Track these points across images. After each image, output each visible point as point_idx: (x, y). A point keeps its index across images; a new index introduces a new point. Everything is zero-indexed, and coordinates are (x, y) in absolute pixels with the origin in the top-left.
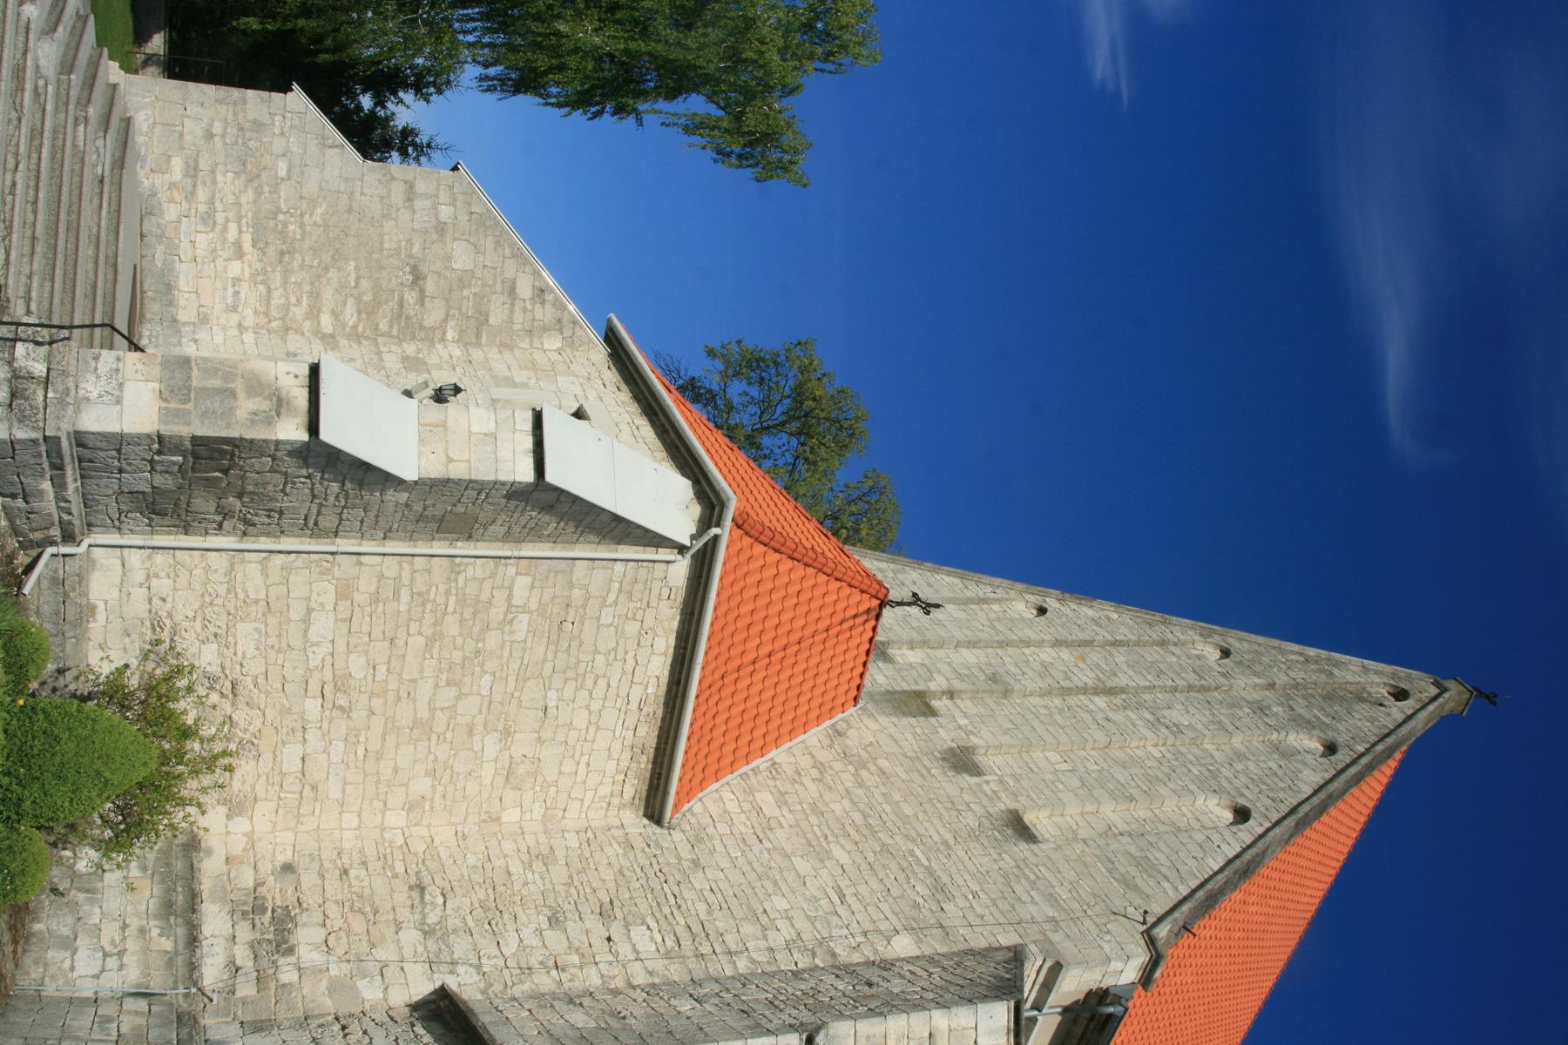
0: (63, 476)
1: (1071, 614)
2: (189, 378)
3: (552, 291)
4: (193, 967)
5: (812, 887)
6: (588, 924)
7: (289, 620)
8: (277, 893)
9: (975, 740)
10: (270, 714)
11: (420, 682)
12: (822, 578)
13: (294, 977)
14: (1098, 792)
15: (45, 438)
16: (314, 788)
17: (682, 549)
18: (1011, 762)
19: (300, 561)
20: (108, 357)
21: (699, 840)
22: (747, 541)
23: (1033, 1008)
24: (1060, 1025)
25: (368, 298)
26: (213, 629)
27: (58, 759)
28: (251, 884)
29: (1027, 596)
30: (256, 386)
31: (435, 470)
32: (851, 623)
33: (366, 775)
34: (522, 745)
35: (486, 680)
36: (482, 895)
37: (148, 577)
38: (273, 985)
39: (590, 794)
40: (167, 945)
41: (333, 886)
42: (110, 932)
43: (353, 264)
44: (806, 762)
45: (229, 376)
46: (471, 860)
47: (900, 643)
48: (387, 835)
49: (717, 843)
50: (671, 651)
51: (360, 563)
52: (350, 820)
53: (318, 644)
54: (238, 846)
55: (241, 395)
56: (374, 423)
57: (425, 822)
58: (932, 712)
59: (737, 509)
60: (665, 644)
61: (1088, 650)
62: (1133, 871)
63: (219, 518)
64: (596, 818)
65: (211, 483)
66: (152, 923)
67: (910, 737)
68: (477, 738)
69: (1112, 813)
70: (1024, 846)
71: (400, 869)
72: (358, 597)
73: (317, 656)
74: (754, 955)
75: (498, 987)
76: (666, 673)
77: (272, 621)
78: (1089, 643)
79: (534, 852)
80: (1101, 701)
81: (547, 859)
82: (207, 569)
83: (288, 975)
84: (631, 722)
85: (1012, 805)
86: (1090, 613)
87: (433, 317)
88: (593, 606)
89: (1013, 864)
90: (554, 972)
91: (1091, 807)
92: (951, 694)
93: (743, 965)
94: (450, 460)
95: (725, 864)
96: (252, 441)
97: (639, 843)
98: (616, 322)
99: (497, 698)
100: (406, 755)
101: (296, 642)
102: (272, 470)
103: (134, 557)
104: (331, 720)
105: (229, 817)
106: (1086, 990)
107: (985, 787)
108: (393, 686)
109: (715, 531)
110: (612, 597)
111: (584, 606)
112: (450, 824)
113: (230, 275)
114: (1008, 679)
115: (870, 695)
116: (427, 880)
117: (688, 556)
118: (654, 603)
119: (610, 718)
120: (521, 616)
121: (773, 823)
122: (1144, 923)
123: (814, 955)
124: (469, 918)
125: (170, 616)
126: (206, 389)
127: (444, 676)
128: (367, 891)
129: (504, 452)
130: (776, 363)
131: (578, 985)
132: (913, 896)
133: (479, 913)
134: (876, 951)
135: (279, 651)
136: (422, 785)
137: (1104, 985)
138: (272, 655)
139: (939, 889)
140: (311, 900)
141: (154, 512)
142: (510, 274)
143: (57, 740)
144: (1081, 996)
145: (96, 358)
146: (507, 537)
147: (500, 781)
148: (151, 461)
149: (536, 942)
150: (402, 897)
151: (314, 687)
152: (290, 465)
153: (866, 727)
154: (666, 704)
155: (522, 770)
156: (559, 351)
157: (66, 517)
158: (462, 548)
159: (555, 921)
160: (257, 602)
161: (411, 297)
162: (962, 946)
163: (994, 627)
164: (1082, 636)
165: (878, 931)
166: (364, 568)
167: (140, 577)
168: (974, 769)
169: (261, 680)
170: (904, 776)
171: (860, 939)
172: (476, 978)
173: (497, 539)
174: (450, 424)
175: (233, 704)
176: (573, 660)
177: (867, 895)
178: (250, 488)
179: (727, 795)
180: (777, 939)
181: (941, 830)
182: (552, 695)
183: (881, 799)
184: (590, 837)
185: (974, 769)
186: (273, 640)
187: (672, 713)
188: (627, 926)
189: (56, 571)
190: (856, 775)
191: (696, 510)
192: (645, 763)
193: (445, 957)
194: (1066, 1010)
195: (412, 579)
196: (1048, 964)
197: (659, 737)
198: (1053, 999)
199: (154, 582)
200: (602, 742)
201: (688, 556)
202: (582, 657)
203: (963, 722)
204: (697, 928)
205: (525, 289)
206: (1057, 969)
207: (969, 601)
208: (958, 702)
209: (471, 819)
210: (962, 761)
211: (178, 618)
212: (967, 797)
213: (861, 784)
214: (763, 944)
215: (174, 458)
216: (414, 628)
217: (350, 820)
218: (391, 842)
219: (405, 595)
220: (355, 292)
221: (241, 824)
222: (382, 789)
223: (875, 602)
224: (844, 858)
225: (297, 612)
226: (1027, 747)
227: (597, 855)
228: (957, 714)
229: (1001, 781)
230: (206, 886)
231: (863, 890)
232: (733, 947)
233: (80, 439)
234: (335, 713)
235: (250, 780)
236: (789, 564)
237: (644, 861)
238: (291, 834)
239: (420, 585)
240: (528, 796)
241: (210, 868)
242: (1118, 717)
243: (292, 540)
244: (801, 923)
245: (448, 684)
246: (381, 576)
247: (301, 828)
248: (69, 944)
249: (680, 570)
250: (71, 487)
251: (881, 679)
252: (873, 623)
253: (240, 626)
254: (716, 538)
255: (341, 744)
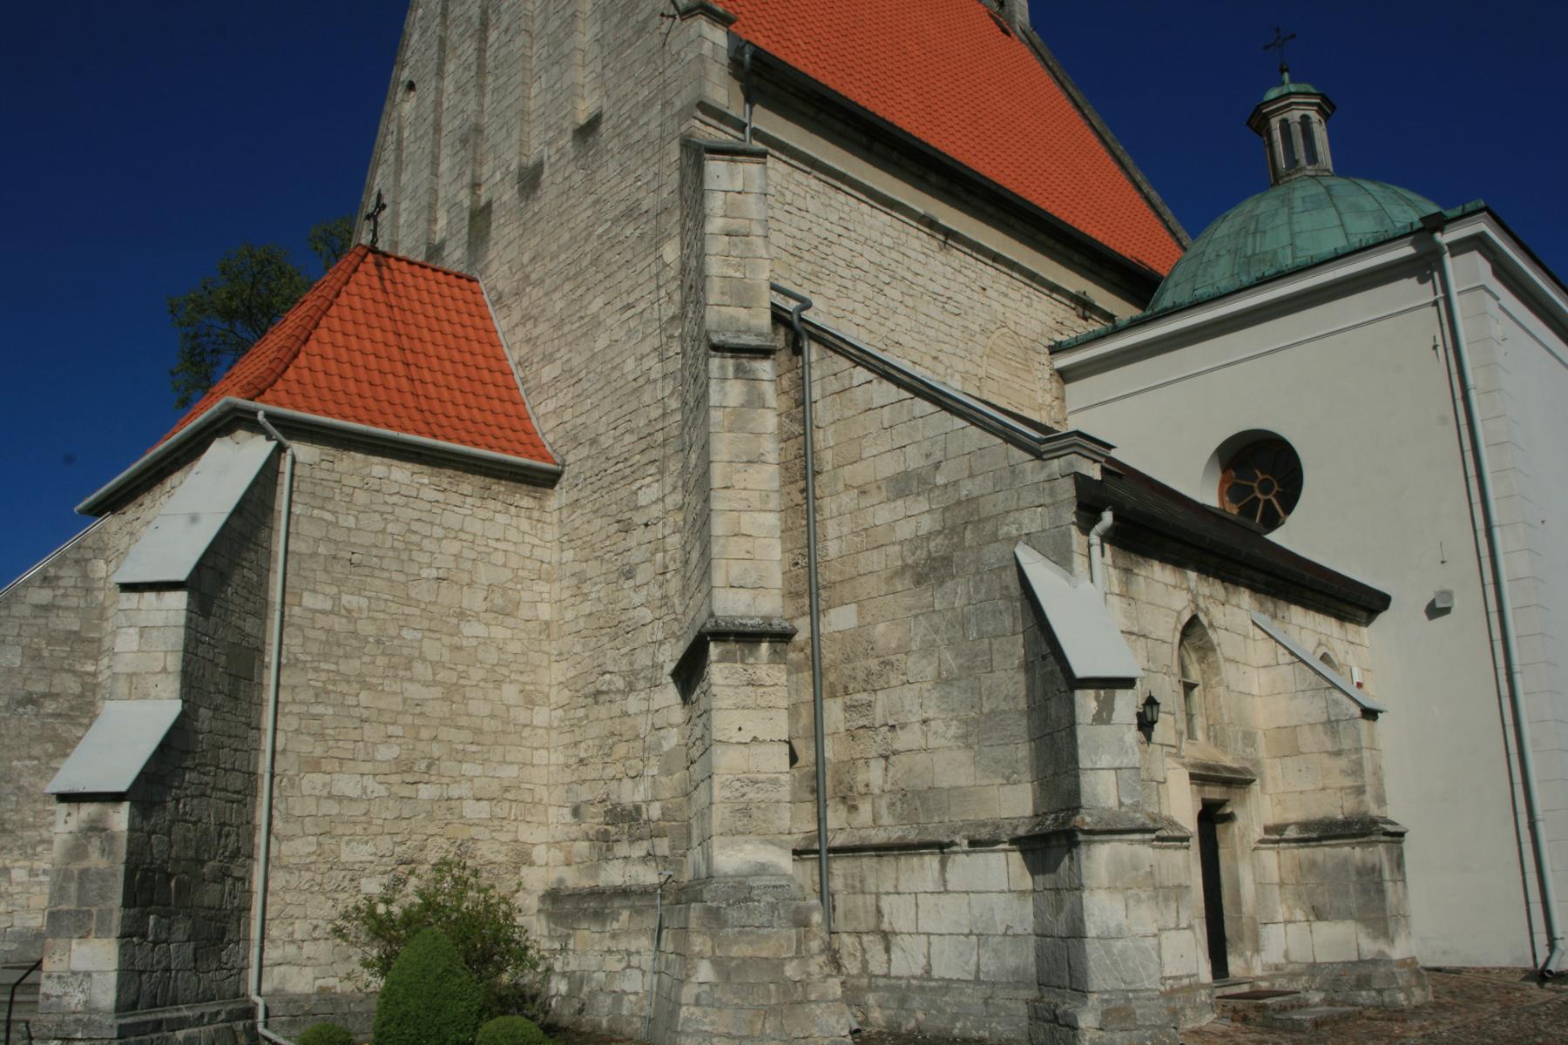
0: (169, 1021)
1: (416, 57)
2: (68, 912)
3: (45, 569)
4: (645, 892)
5: (620, 334)
6: (633, 544)
7: (339, 814)
8: (594, 821)
9: (514, 167)
10: (431, 830)
11: (406, 694)
12: (334, 311)
13: (657, 805)
14: (566, 49)
15: (119, 1037)
16: (507, 790)
17: (280, 449)
18: (536, 132)
19: (280, 806)
20: (48, 987)
21: (575, 438)
22: (280, 385)
23: (743, 132)
24: (765, 106)
25: (50, 748)
26: (346, 883)
27: (421, 1013)
28: (586, 844)
29: (398, 99)
30: (77, 850)
31: (172, 685)
32: (387, 283)
33: (496, 743)
34: (474, 601)
35: (407, 634)
36: (605, 639)
37: (293, 942)
38: (662, 824)
39: (528, 539)
40: (625, 914)
41: (590, 772)
42: (613, 964)
43: (15, 763)
44: (520, 333)
45: (67, 876)
46: (578, 648)
47: (430, 231)
48: (556, 724)
49: (579, 421)
50: (386, 460)
51: (284, 751)
52: (540, 757)
53: (364, 789)
54: (557, 855)
55: (85, 864)
56: (124, 735)
57: (546, 690)
58: (489, 204)
59: (238, 395)
60: (378, 467)
61: (449, 44)
62: (632, 21)
63: (229, 881)
64: (551, 533)
65: (183, 889)
66: (608, 928)
67: (507, 230)
68: (465, 643)
69: (585, 35)
70: (603, 128)
71: (581, 713)
72: (319, 751)
73: (375, 788)
74: (667, 392)
75: (676, 626)
76: (409, 465)
77: (339, 830)
78: (442, 42)
79: (575, 591)
80: (493, 36)
81: (581, 579)
82: (286, 889)
83: (655, 811)
84: (456, 499)
85: (569, 136)
86: (416, 37)
87: (72, 685)
88: (335, 534)
89: (616, 140)
90: (668, 576)
91: (578, 57)
92: (475, 186)
93: (674, 404)
94: (164, 670)
95: (596, 415)
96: (130, 853)
97: (574, 494)
98: (81, 506)
99: (425, 624)
100: (478, 707)
101: (362, 807)
102: (169, 834)
103: (272, 954)
104: (440, 775)
105: (532, 864)
106: (730, 78)
107: (553, 160)
108: (409, 719)
109: (260, 417)
110: (329, 517)
111: (336, 542)
112: (549, 667)
113: (26, 879)
114: (466, 127)
115: (471, 265)
116: (591, 688)
117: (288, 443)
118: (337, 477)
119: (452, 519)
120: (344, 601)
121: (567, 367)
122: (674, 17)
123: (671, 337)
124: (623, 651)
125: (331, 921)
126: (79, 898)
127: (401, 673)
128: (597, 742)
129: (158, 619)
130: (196, 336)
131: (678, 555)
132: (633, 239)
133: (618, 643)
134: (674, 278)
135: (370, 823)
136: (510, 693)
137: (726, 61)
138: (374, 829)
139: (631, 213)
140: (600, 791)
141: (222, 939)
142: (27, 611)
143: (406, 1014)
144: (737, 85)
145: (48, 997)
146: (262, 615)
147: (509, 621)
148: (155, 943)
149: (644, 591)
150: (602, 711)
151: (407, 791)
152: (161, 818)
153: (496, 275)
154: (440, 466)
155: (499, 601)
156: (108, 562)
157: (223, 1016)
158: (271, 657)
159: (629, 574)
160: (320, 844)
161: (50, 707)
162: (676, 196)
163: (422, 137)
164: (435, 48)
165: (657, 275)
166: (289, 747)
167: (291, 950)
168: (539, 167)
169: (398, 839)
170: (538, 238)
171: (663, 293)
172: (667, 646)
173: (264, 623)
174: (129, 670)
175: (421, 863)
176: (391, 553)
177: (629, 283)
178: (191, 853)
179: (541, 410)
180: (657, 371)
181: (584, 206)
182: (425, 573)
183: (555, 262)
184: (567, 540)
185: (539, 167)
186: (359, 829)
187: (137, 487)
188: (637, 508)
189: (282, 1023)
190: (534, 285)
191: (241, 434)
192: (500, 487)
193: (648, 673)
194: (750, 99)
195: (302, 703)
196: (699, 114)
197: (474, 473)
198: (737, 109)
199: (298, 936)
200: (476, 527)
201: (288, 443)
202: (388, 545)
203: (498, 176)
204: (643, 444)
205: (44, 596)
206: (705, 108)
207: (398, 159)
208: (484, 178)
209: (546, 648)
210: (530, 180)
211: (334, 914)
212: (559, 179)
213: (542, 281)
214: (659, 384)
215: (151, 923)
216: (351, 701)
217: (540, 757)
218: (562, 720)
219: (319, 709)
220: (44, 760)
221: (540, 854)
222: (511, 728)
223: (370, 258)
224: (599, 302)
225: (332, 808)
226: (523, 114)
227: (581, 533)
228: (491, 182)
229: (549, 144)
230: (586, 883)
231: (626, 285)
232: (660, 411)
233: (122, 1007)
234: (433, 772)
235: (497, 846)
236: (313, 344)
237: (588, 492)
238: (552, 810)
239: (308, 695)
240: (526, 596)
241: (574, 879)
242: (506, 19)
243: (258, 814)
244: (646, 348)
245: (409, 669)
246: (298, 731)
247: (545, 800)
248: (619, 997)
249: (303, 451)
250: (186, 1013)
251: (457, 254)
252: (392, 261)
253: (343, 859)
254: (268, 416)
255: (465, 766)
